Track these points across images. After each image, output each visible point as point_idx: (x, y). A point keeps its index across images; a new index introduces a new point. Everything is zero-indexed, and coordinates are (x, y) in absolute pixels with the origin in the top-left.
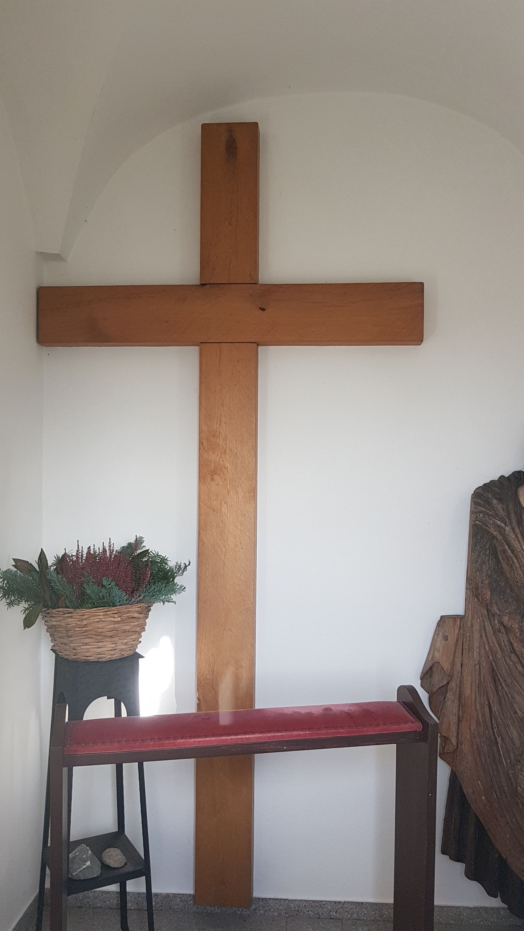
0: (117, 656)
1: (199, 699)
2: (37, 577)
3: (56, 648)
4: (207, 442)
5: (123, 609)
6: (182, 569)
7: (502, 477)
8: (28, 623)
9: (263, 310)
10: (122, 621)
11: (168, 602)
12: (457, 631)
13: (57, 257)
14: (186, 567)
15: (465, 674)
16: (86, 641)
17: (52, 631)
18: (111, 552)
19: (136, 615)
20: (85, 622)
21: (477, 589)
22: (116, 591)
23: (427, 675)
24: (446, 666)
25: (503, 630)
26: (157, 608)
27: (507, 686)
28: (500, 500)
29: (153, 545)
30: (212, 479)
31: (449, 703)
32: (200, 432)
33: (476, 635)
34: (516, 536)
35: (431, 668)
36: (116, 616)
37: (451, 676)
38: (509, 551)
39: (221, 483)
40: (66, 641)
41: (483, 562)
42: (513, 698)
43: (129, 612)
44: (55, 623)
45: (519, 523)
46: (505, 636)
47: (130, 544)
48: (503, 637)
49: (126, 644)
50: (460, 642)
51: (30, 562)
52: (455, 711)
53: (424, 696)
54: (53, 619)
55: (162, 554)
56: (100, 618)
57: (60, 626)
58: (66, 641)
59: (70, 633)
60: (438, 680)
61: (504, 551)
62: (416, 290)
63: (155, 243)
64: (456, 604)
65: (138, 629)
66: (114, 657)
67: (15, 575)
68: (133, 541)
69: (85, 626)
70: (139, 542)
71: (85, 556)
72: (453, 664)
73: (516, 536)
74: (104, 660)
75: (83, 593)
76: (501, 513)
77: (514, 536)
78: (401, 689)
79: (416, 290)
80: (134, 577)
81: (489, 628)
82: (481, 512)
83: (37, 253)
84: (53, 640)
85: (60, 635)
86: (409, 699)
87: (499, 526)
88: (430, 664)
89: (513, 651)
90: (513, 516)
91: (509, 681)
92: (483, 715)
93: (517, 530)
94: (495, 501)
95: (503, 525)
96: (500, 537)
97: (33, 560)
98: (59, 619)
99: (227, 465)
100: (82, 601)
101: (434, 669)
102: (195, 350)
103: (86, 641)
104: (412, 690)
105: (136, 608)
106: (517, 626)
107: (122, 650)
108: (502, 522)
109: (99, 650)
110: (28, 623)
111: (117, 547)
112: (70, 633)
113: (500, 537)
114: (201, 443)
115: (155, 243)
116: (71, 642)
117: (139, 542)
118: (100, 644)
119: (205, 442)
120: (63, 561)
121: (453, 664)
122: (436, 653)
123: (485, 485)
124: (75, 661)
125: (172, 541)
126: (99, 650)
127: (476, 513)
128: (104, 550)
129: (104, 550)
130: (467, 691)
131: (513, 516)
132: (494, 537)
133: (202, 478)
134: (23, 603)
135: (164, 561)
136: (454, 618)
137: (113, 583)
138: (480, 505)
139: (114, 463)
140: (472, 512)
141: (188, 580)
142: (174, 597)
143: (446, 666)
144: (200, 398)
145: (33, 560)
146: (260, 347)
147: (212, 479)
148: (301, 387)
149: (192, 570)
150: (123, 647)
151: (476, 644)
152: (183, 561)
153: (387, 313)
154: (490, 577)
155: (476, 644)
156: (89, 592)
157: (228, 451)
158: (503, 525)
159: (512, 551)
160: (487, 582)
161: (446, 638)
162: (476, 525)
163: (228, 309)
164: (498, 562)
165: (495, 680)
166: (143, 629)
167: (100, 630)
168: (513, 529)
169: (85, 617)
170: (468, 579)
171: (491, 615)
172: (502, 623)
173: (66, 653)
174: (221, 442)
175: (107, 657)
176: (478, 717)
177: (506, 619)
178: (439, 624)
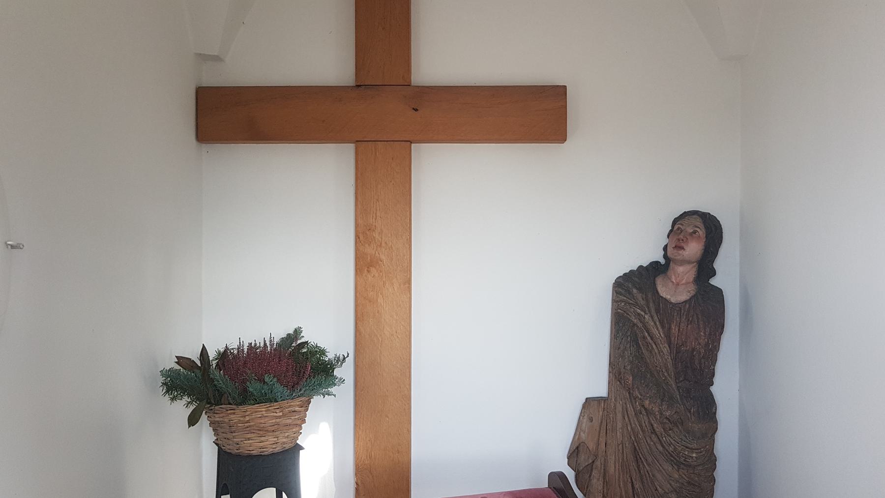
0: (278, 449)
1: (357, 484)
2: (199, 374)
3: (219, 442)
4: (363, 235)
5: (284, 403)
6: (340, 360)
7: (641, 267)
8: (193, 420)
9: (416, 110)
10: (284, 415)
11: (329, 395)
12: (601, 413)
13: (217, 59)
14: (344, 358)
15: (608, 453)
16: (249, 436)
17: (215, 426)
18: (272, 345)
19: (297, 409)
20: (247, 418)
21: (620, 374)
22: (278, 388)
23: (574, 454)
24: (592, 446)
25: (644, 412)
26: (317, 402)
27: (649, 465)
28: (640, 290)
29: (310, 336)
30: (368, 271)
31: (594, 481)
32: (357, 226)
33: (619, 416)
34: (655, 323)
35: (577, 448)
36: (278, 411)
37: (596, 456)
38: (649, 338)
39: (377, 275)
40: (229, 436)
41: (625, 349)
42: (653, 476)
43: (290, 406)
44: (218, 419)
45: (658, 311)
46: (646, 418)
47: (289, 335)
48: (644, 419)
49: (287, 437)
50: (604, 424)
51: (193, 359)
52: (600, 488)
53: (570, 475)
54: (217, 416)
55: (322, 345)
56: (261, 414)
57: (223, 422)
58: (229, 436)
59: (233, 429)
60: (584, 460)
61: (644, 338)
62: (558, 93)
63: (320, 54)
64: (598, 385)
65: (299, 422)
66: (276, 450)
67: (177, 372)
68: (291, 332)
69: (248, 422)
70: (297, 332)
71: (246, 350)
72: (598, 444)
73: (655, 323)
74: (266, 453)
75: (245, 390)
76: (642, 302)
77: (652, 324)
78: (552, 476)
79: (558, 93)
80: (295, 369)
81: (631, 412)
82: (622, 301)
83: (199, 55)
84: (216, 433)
85: (222, 430)
86: (560, 485)
87: (639, 314)
88: (577, 444)
89: (654, 431)
90: (651, 305)
91: (650, 459)
92: (626, 492)
93: (656, 318)
94: (635, 291)
95: (643, 313)
96: (640, 325)
97: (195, 356)
98: (221, 415)
99: (383, 257)
100: (245, 398)
101: (581, 449)
102: (351, 147)
103: (249, 436)
104: (562, 476)
105: (297, 402)
106: (657, 409)
107: (284, 443)
108: (642, 310)
109: (261, 444)
110: (193, 420)
111: (276, 340)
112: (233, 429)
113: (640, 325)
114: (357, 237)
115: (320, 54)
116: (234, 437)
117: (297, 332)
118: (263, 439)
119: (361, 238)
120: (224, 356)
121: (598, 444)
122: (582, 434)
123: (625, 274)
124: (238, 456)
125: (330, 331)
126: (261, 444)
127: (617, 302)
128: (265, 344)
129: (265, 344)
130: (611, 470)
131: (651, 305)
132: (634, 325)
133: (358, 270)
134: (186, 398)
135: (323, 352)
136: (599, 400)
137: (275, 379)
138: (621, 294)
139: (274, 261)
140: (614, 301)
141: (345, 372)
142: (333, 390)
143: (592, 446)
144: (356, 193)
145: (195, 356)
146: (413, 145)
147: (368, 271)
148: (460, 193)
149: (350, 361)
150: (285, 440)
151: (619, 425)
152: (341, 353)
153: (533, 114)
154: (631, 362)
155: (619, 425)
156: (251, 390)
157: (383, 244)
158: (643, 313)
159: (652, 339)
160: (629, 368)
161: (591, 420)
162: (618, 313)
163: (380, 109)
164: (639, 347)
165: (637, 460)
166: (304, 421)
167: (262, 425)
168: (652, 317)
169: (248, 413)
170: (611, 364)
171: (632, 398)
172: (643, 406)
173: (228, 447)
174: (376, 235)
175: (269, 451)
176: (621, 494)
177: (647, 402)
178: (584, 406)
